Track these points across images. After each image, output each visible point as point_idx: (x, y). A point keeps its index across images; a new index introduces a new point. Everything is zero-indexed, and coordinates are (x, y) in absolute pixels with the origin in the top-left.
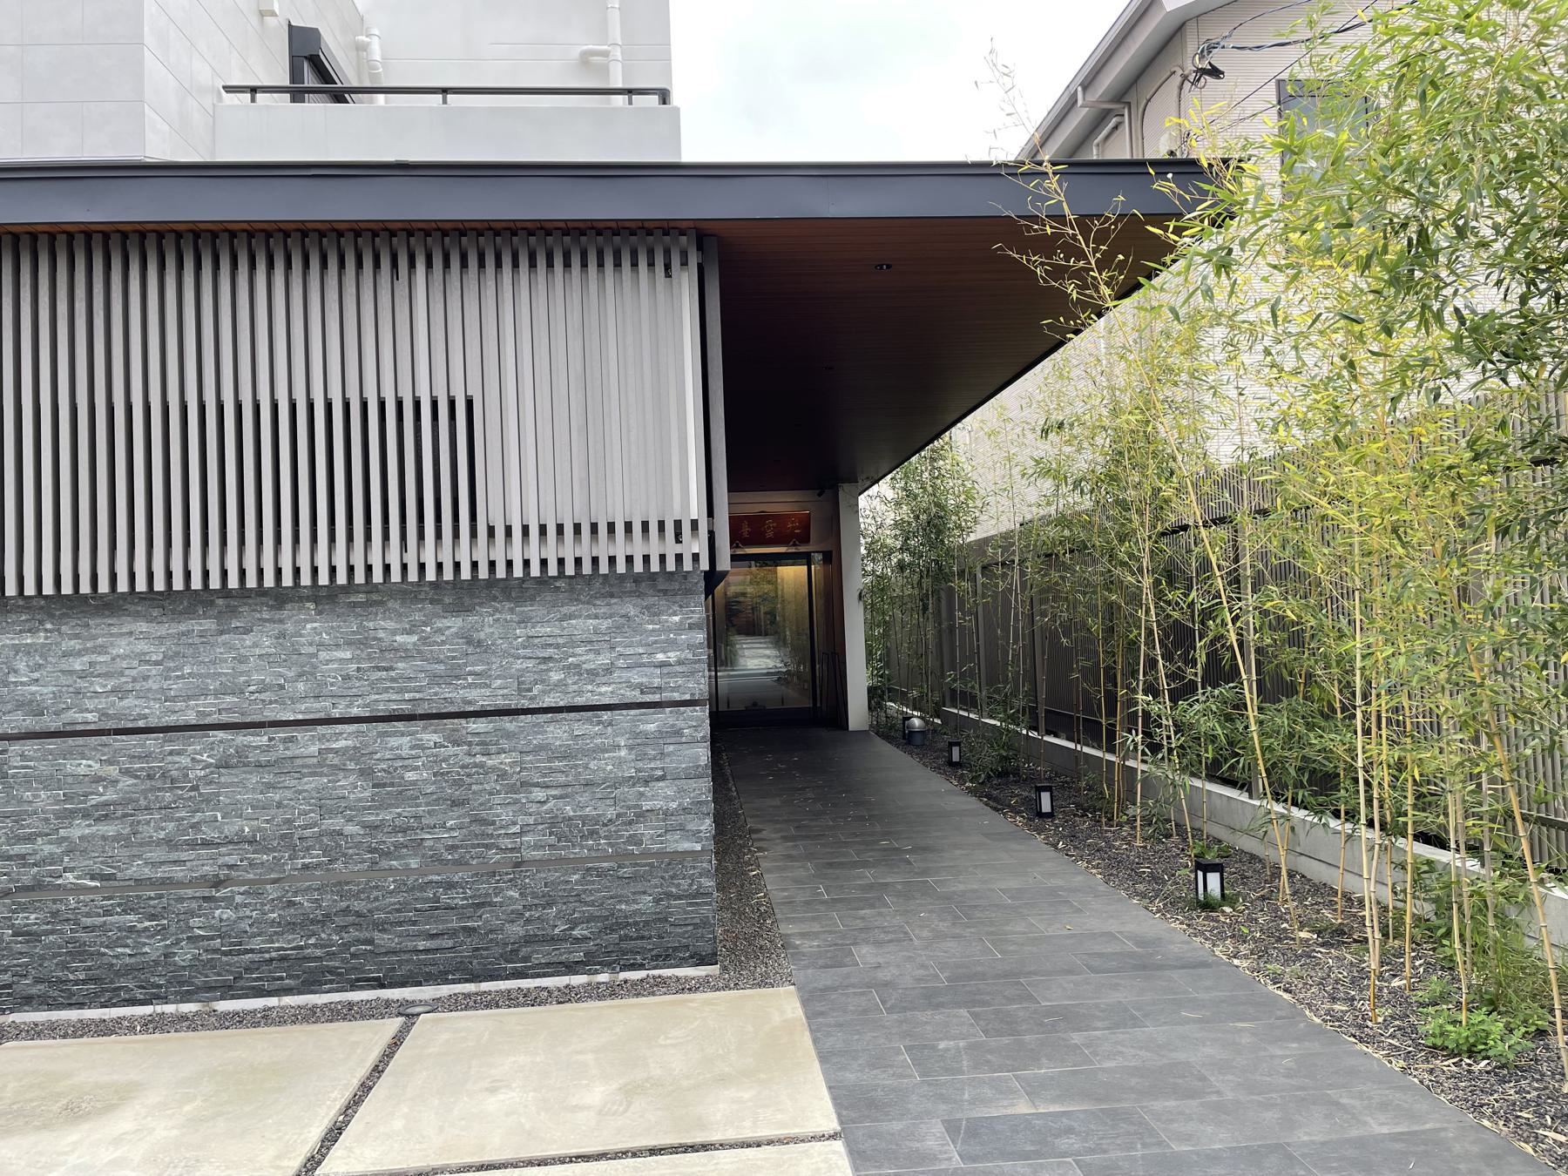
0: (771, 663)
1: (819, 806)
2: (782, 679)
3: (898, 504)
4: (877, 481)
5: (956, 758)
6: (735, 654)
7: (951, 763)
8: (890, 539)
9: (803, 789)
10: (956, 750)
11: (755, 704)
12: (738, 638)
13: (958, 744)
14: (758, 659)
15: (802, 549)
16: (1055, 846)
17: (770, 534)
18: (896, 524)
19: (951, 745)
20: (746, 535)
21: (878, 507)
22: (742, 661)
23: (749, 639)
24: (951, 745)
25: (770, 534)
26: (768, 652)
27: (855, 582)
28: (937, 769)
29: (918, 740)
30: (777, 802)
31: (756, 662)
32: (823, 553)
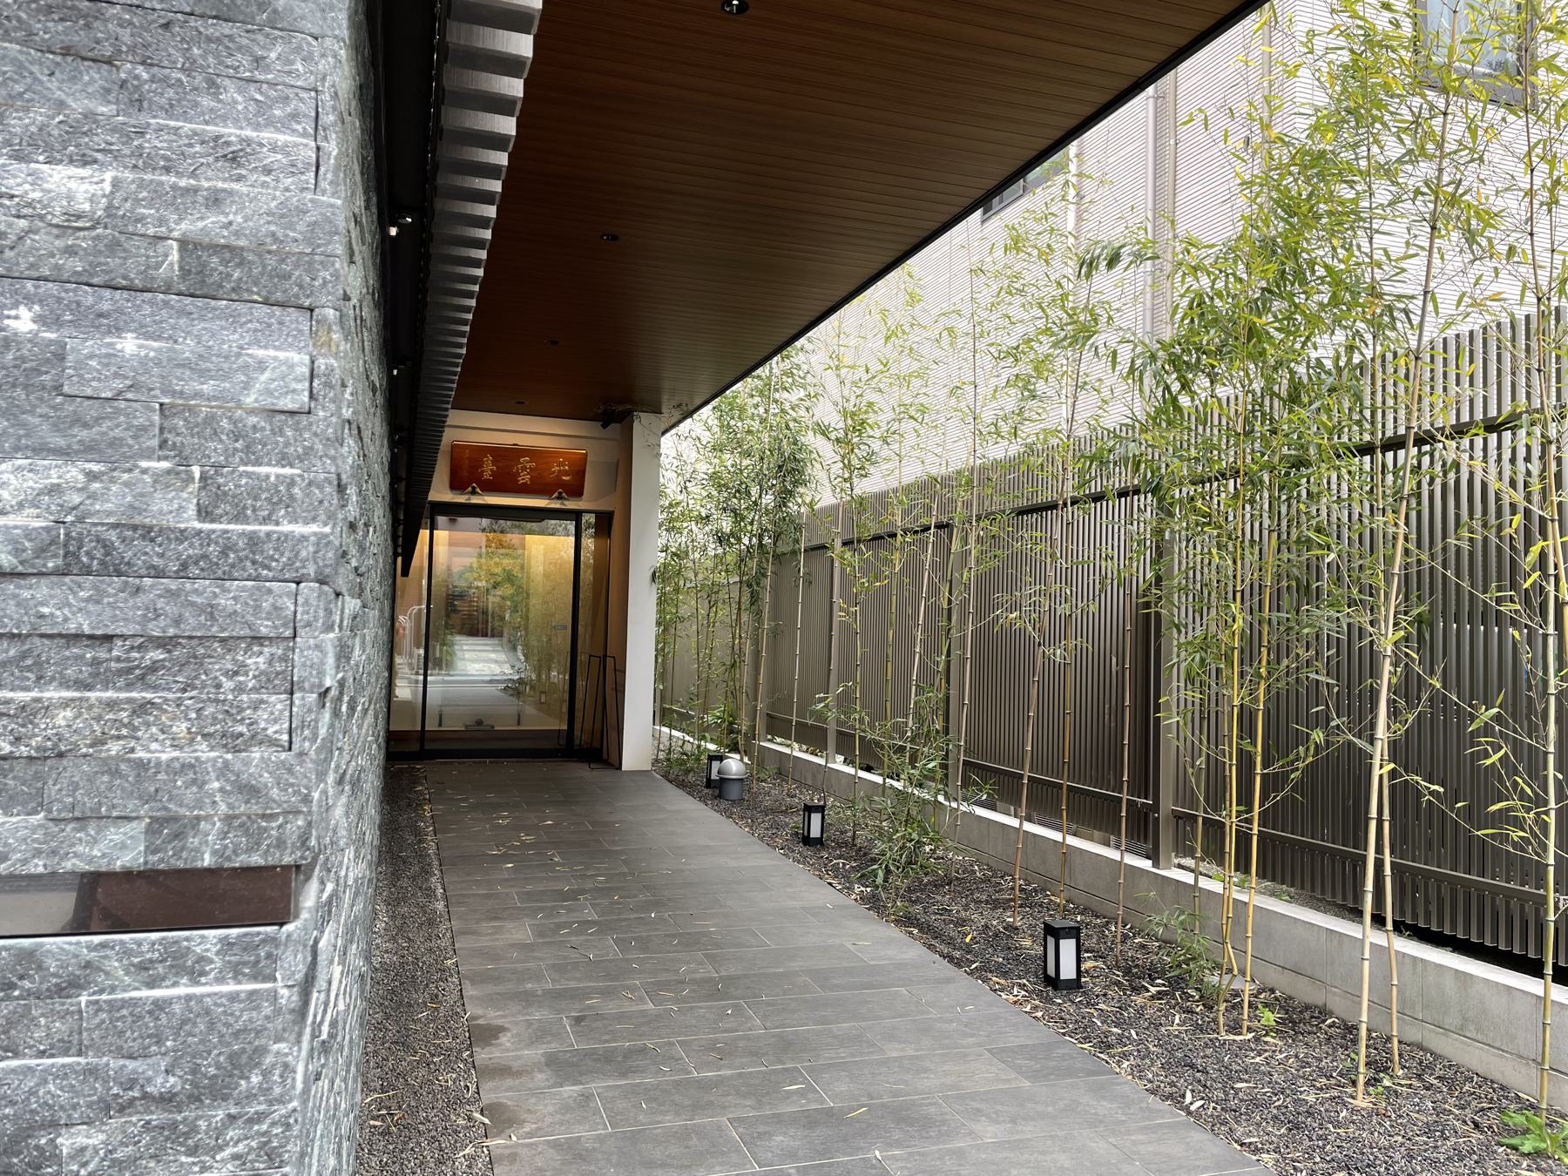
0: (496, 669)
1: (609, 947)
2: (515, 689)
3: (718, 448)
4: (690, 414)
5: (815, 832)
6: (452, 654)
7: (807, 840)
8: (698, 498)
9: (573, 895)
10: (816, 819)
11: (479, 723)
12: (458, 638)
13: (821, 809)
14: (480, 667)
15: (571, 505)
16: (1176, 1099)
17: (524, 478)
18: (714, 477)
19: (809, 809)
20: (487, 475)
21: (684, 457)
22: (460, 664)
23: (471, 640)
24: (809, 809)
25: (524, 478)
26: (493, 656)
27: (648, 550)
28: (787, 850)
29: (734, 792)
30: (520, 932)
31: (477, 666)
32: (599, 514)
